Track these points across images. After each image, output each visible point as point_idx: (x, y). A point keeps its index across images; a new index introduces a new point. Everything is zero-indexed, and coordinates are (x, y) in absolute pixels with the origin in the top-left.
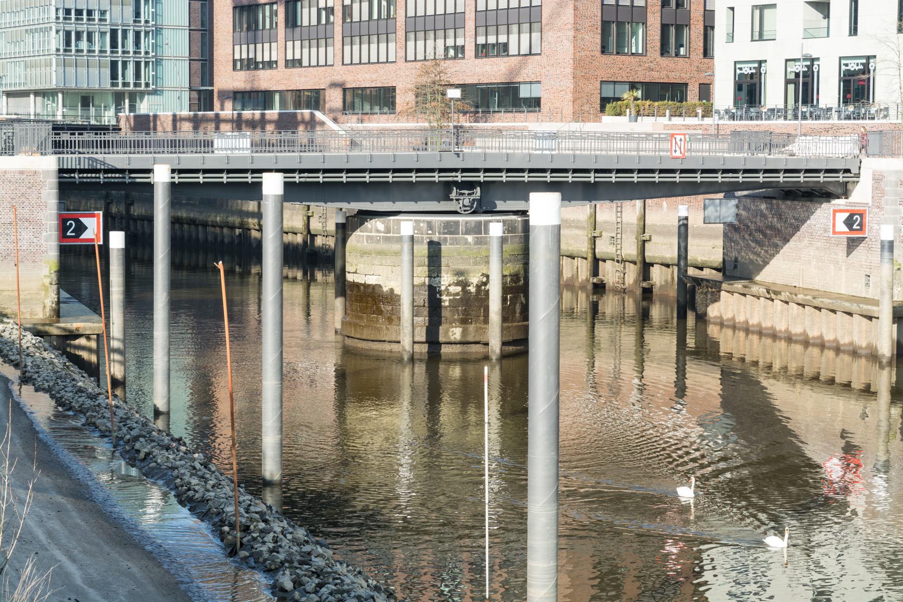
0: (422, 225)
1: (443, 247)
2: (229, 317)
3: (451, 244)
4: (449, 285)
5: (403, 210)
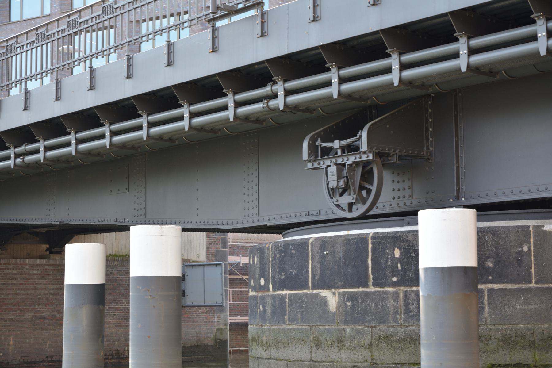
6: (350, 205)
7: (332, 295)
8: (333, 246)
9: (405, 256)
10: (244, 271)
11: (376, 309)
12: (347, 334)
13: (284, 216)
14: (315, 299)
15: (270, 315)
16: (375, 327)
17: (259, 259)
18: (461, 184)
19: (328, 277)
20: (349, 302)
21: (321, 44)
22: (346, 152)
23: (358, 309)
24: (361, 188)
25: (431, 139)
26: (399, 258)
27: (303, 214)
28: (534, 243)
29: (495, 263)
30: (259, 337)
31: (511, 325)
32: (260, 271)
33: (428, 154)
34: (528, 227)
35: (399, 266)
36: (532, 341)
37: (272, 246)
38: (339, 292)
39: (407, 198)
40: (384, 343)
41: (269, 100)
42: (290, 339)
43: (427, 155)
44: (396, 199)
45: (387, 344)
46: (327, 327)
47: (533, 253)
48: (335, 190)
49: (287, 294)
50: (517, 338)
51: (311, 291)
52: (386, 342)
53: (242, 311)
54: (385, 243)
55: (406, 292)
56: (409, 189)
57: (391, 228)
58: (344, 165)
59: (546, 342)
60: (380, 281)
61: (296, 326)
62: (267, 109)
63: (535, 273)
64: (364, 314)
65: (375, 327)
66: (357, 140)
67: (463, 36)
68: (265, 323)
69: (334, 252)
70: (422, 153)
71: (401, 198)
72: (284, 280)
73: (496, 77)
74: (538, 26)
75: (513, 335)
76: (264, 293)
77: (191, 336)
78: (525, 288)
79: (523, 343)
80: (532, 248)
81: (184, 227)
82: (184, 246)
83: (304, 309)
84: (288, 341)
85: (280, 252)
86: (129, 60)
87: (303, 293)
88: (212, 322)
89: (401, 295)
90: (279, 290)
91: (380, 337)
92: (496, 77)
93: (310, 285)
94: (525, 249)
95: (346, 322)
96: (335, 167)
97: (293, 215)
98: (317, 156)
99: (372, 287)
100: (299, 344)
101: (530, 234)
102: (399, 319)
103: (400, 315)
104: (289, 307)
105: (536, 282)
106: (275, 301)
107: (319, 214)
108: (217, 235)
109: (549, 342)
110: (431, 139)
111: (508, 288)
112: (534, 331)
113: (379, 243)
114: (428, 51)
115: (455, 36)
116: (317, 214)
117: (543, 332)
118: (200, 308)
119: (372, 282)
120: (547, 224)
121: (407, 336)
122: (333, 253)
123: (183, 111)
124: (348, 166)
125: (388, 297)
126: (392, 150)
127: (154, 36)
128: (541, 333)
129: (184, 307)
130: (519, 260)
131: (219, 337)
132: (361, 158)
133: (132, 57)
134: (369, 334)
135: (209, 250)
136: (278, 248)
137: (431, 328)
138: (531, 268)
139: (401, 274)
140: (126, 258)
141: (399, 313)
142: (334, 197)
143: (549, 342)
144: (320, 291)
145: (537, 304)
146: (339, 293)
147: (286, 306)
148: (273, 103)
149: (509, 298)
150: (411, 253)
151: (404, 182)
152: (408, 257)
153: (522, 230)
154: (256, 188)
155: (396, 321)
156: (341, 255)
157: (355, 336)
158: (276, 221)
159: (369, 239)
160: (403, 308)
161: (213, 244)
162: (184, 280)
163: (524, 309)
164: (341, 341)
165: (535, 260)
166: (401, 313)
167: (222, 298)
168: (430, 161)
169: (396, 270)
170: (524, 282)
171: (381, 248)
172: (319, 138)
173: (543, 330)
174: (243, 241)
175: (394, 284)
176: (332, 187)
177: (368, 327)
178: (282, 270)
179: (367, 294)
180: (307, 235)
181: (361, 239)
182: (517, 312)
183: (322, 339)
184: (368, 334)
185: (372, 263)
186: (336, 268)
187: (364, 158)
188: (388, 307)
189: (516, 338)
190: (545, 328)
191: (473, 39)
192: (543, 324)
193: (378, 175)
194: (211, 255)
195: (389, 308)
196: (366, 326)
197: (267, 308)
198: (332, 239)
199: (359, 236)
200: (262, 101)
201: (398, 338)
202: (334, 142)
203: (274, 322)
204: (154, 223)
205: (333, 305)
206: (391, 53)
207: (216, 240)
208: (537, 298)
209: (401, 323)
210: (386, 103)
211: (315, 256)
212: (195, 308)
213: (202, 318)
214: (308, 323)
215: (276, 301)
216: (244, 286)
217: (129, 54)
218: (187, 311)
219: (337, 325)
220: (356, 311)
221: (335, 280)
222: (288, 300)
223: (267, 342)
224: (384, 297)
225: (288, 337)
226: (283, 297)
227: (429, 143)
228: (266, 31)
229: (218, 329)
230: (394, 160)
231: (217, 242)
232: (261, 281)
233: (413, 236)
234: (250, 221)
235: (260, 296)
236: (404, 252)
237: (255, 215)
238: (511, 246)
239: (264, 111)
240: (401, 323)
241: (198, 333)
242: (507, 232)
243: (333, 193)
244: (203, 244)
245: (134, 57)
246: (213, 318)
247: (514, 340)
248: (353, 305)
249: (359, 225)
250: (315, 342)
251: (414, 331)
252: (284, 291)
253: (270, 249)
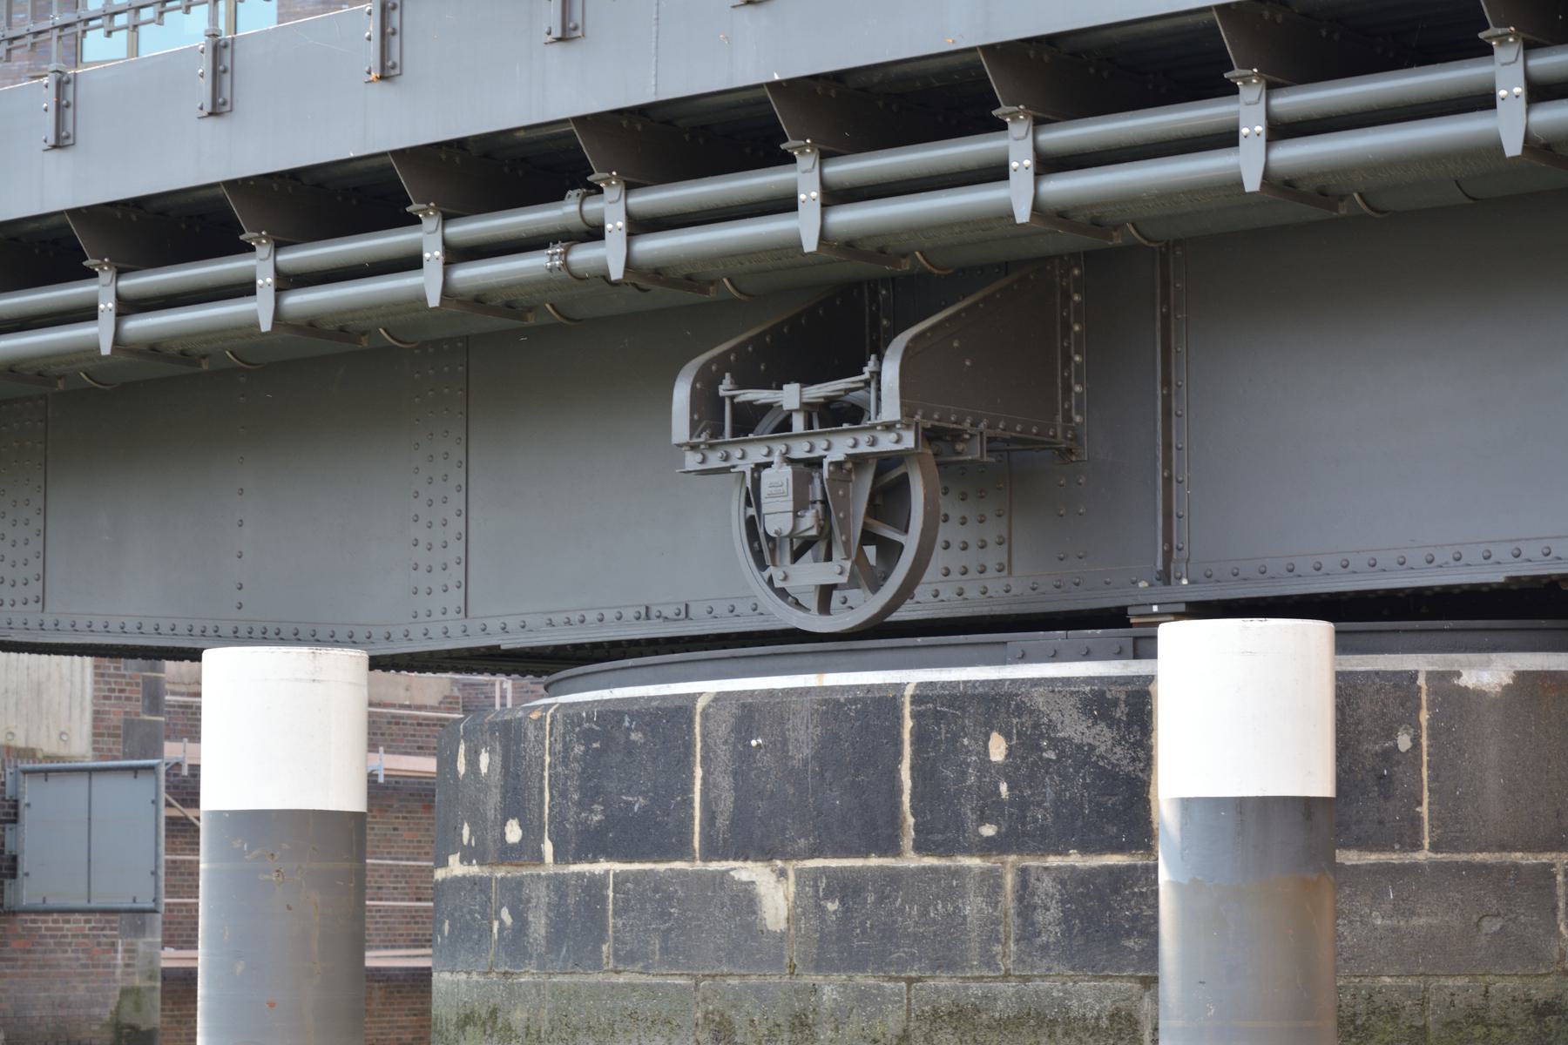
6: (826, 592)
7: (773, 877)
8: (782, 720)
9: (1024, 759)
10: (187, 794)
11: (924, 924)
12: (823, 1004)
13: (559, 619)
14: (714, 891)
15: (543, 942)
16: (919, 979)
17: (498, 759)
18: (1178, 530)
19: (760, 818)
20: (833, 902)
21: (776, 77)
22: (816, 423)
23: (863, 924)
24: (868, 537)
25: (1078, 389)
26: (1004, 765)
27: (629, 614)
28: (1431, 727)
30: (494, 1013)
31: (1355, 976)
32: (504, 797)
33: (1069, 436)
34: (1413, 676)
35: (1004, 788)
36: (1418, 1028)
37: (553, 716)
38: (801, 870)
39: (991, 572)
40: (950, 1030)
41: (572, 245)
42: (618, 1018)
43: (1066, 438)
44: (955, 575)
45: (958, 1034)
46: (753, 980)
47: (1425, 758)
48: (778, 543)
49: (611, 873)
50: (1373, 1018)
51: (699, 865)
52: (955, 1028)
53: (176, 929)
54: (958, 717)
55: (1023, 872)
56: (1000, 544)
57: (969, 669)
58: (816, 463)
59: (1460, 1029)
60: (939, 837)
61: (644, 976)
62: (564, 273)
63: (1431, 819)
64: (882, 938)
65: (919, 979)
66: (862, 385)
67: (1254, 81)
68: (521, 968)
69: (785, 742)
70: (1051, 433)
71: (973, 574)
72: (601, 830)
73: (1337, 211)
74: (1497, 64)
75: (1362, 1007)
76: (520, 869)
77: (35, 1013)
78: (1400, 864)
79: (1392, 1033)
80: (1424, 742)
81: (371, 654)
82: (17, 704)
83: (672, 922)
84: (611, 1025)
85: (588, 737)
86: (61, 85)
87: (671, 869)
88: (108, 966)
89: (1009, 881)
90: (578, 859)
91: (935, 1011)
92: (1337, 211)
93: (697, 844)
94: (1404, 742)
95: (820, 965)
96: (788, 471)
97: (591, 617)
98: (718, 432)
99: (911, 854)
100: (652, 1034)
101: (1420, 699)
102: (999, 957)
103: (1005, 944)
104: (616, 913)
105: (1435, 847)
106: (563, 896)
107: (683, 615)
108: (130, 667)
109: (1469, 1030)
110: (1078, 389)
111: (1348, 863)
112: (1424, 998)
113: (939, 717)
114: (1131, 118)
115: (1228, 80)
116: (678, 614)
117: (1453, 1001)
118: (67, 917)
119: (914, 840)
120: (1470, 666)
121: (1026, 1011)
122: (779, 745)
123: (254, 267)
124: (831, 468)
125: (964, 887)
126: (968, 421)
127: (161, 13)
128: (1447, 1004)
129: (14, 913)
130: (1383, 777)
131: (129, 1017)
132: (873, 443)
133: (72, 77)
134: (900, 1002)
135: (102, 720)
136: (580, 725)
137: (1200, 982)
138: (1420, 803)
139: (1011, 815)
141: (1002, 936)
142: (774, 565)
143: (1469, 1030)
144: (731, 864)
145: (1437, 915)
146: (800, 874)
147: (605, 910)
148: (583, 255)
149: (1349, 895)
150: (1045, 751)
151: (981, 522)
152: (1035, 763)
153: (1395, 686)
154: (458, 524)
155: (989, 961)
156: (807, 752)
157: (852, 1009)
158: (532, 634)
159: (903, 703)
160: (1013, 922)
161: (117, 698)
162: (15, 822)
163: (1394, 930)
164: (802, 1024)
165: (1431, 779)
166: (1007, 938)
167: (157, 887)
168: (1074, 459)
169: (993, 802)
170: (1397, 847)
171: (943, 731)
172: (727, 375)
173: (1453, 995)
174: (183, 689)
175: (987, 847)
176: (776, 532)
177: (897, 979)
178: (590, 795)
179: (894, 878)
180: (673, 685)
181: (879, 701)
182: (1376, 938)
183: (739, 1019)
184: (896, 1002)
185: (913, 778)
186: (791, 791)
187: (887, 443)
188: (965, 917)
189: (1369, 1019)
190: (1459, 988)
191: (1284, 90)
192: (1454, 976)
193: (925, 498)
194: (110, 735)
195: (969, 920)
196: (891, 979)
197: (530, 919)
198: (777, 700)
199: (869, 691)
200: (547, 247)
201: (997, 1015)
202: (781, 389)
203: (560, 963)
204: (279, 639)
205: (777, 909)
206: (1008, 120)
207: (128, 684)
208: (1435, 895)
209: (1007, 970)
210: (951, 271)
211: (715, 752)
212: (50, 918)
213: (73, 951)
214: (689, 968)
215: (567, 895)
216: (187, 843)
217: (62, 67)
218: (24, 928)
219: (792, 974)
220: (858, 931)
221: (784, 829)
222: (615, 891)
223: (528, 1028)
224: (951, 887)
225: (612, 1012)
226: (595, 886)
227: (1070, 401)
228: (580, 23)
229: (125, 992)
230: (973, 452)
231: (131, 692)
232: (508, 829)
233: (1051, 695)
234: (435, 631)
235: (502, 878)
236: (1023, 744)
237: (451, 614)
238: (1360, 733)
239: (550, 280)
240: (1007, 970)
241: (60, 1005)
242: (1349, 691)
243: (773, 552)
244: (83, 697)
245: (79, 79)
246: (108, 951)
247: (1363, 1025)
248: (846, 911)
249: (854, 658)
250: (712, 1026)
251: (1048, 993)
252: (598, 862)
253: (548, 728)
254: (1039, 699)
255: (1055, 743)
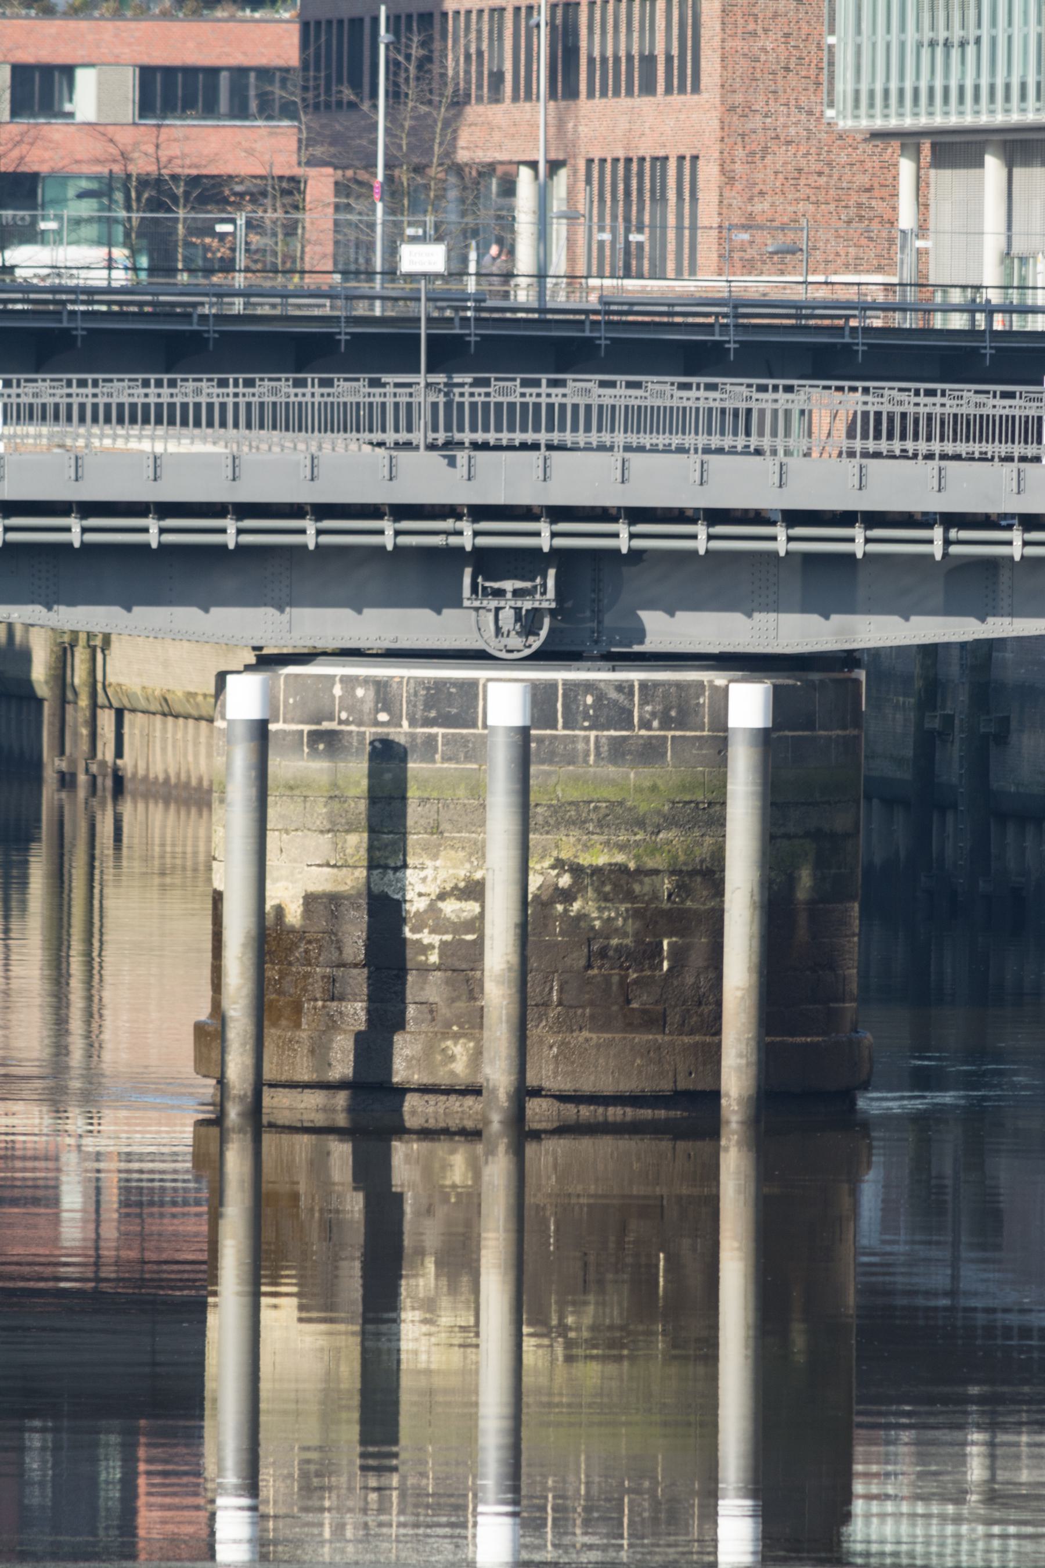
0: (360, 692)
1: (413, 766)
2: (714, 1024)
3: (446, 759)
4: (442, 896)
5: (322, 644)
29: (679, 713)
55: (597, 737)
96: (512, 611)
140: (365, 1440)
155: (586, 762)
179: (555, 737)
254: (602, 685)
255: (608, 699)
